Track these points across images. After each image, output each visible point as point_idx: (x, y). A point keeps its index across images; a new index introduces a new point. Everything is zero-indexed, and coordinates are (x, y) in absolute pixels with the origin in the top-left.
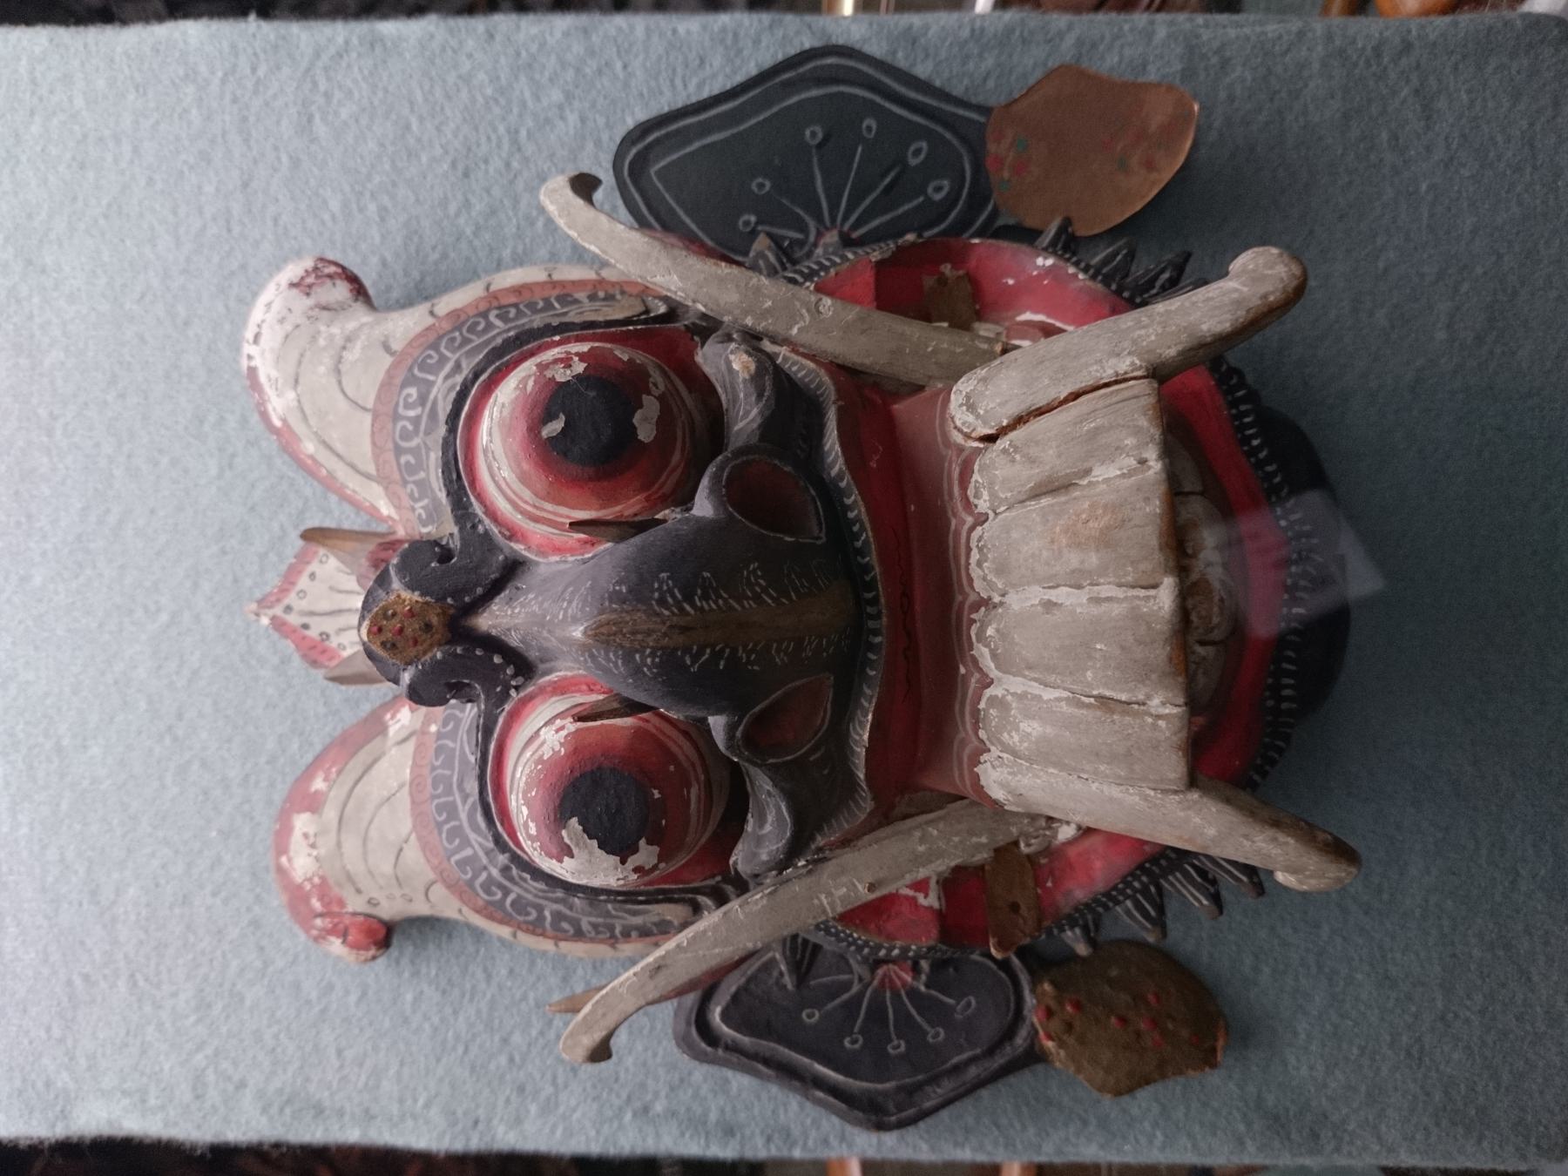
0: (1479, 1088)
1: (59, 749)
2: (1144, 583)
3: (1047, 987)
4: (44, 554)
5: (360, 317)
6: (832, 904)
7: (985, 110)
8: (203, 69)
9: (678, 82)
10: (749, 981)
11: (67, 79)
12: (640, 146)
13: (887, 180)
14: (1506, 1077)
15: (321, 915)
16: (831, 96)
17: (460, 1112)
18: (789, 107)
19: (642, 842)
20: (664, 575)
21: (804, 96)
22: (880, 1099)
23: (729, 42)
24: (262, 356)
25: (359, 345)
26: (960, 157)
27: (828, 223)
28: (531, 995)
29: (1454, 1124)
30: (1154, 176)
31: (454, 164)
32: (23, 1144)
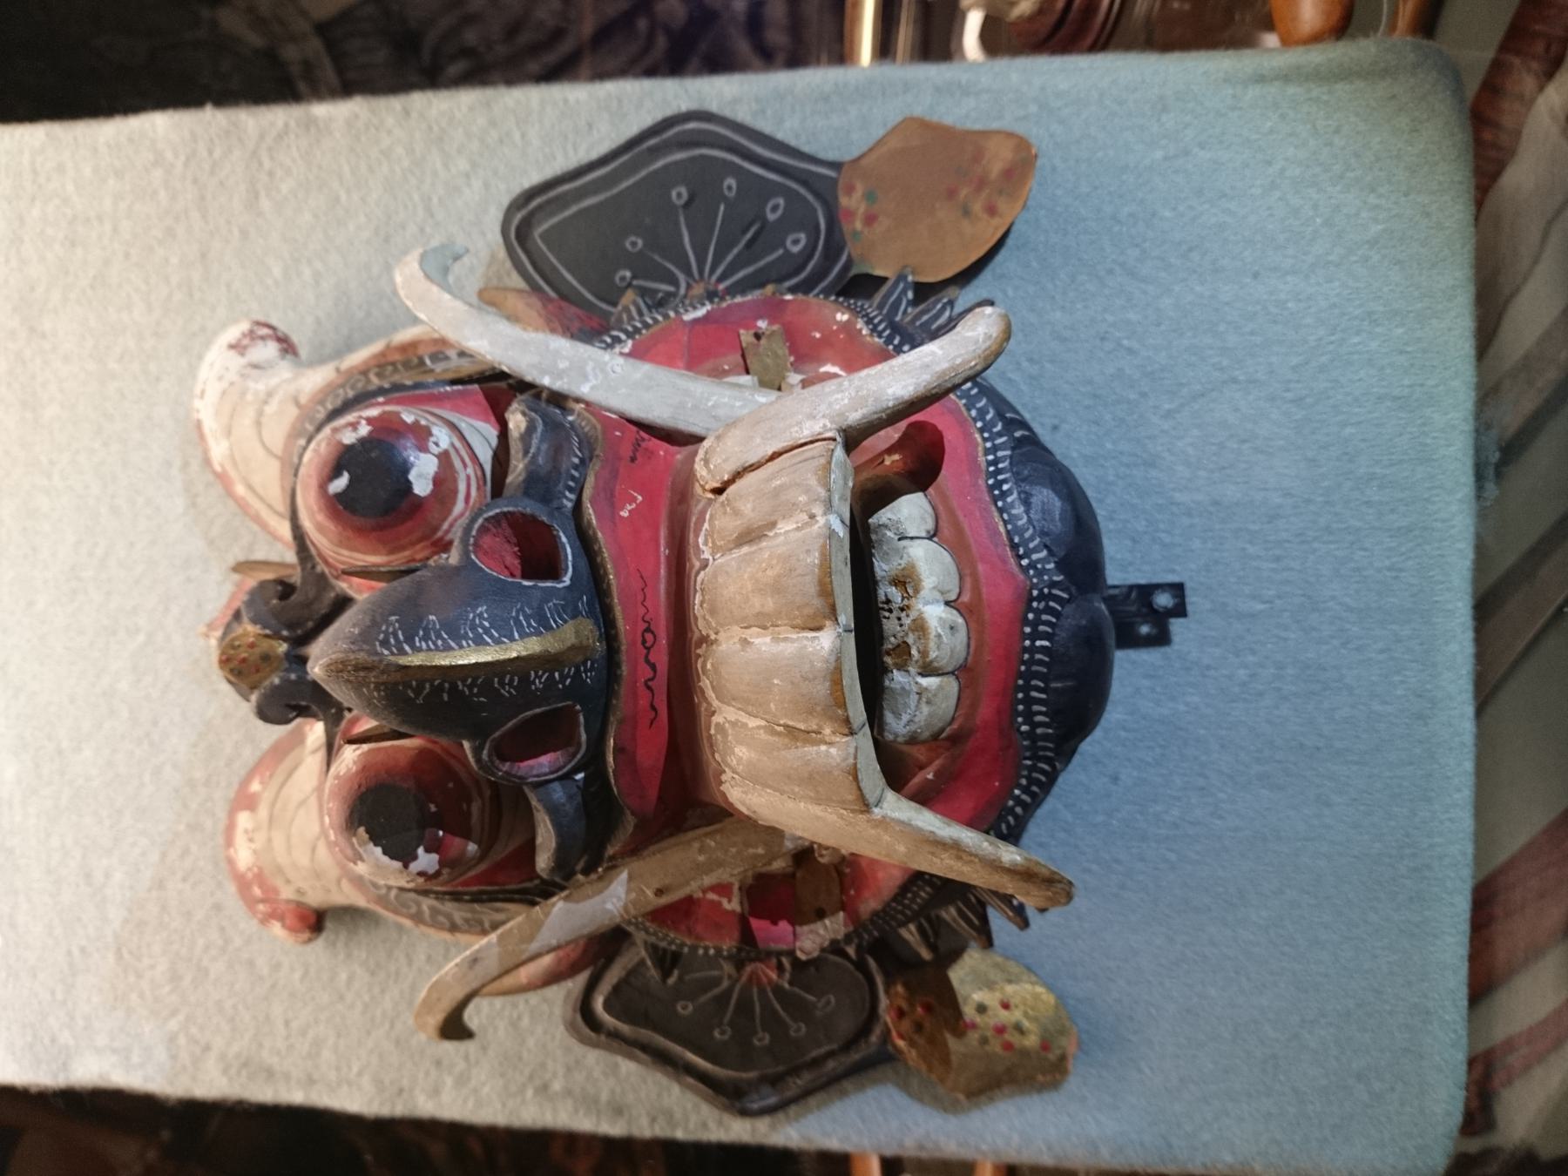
1: (60, 752)
3: (900, 989)
7: (836, 166)
8: (169, 155)
9: (570, 147)
11: (61, 169)
13: (749, 235)
15: (262, 901)
16: (692, 159)
18: (656, 172)
19: (421, 850)
20: (393, 618)
26: (815, 210)
27: (696, 275)
32: (33, 1090)
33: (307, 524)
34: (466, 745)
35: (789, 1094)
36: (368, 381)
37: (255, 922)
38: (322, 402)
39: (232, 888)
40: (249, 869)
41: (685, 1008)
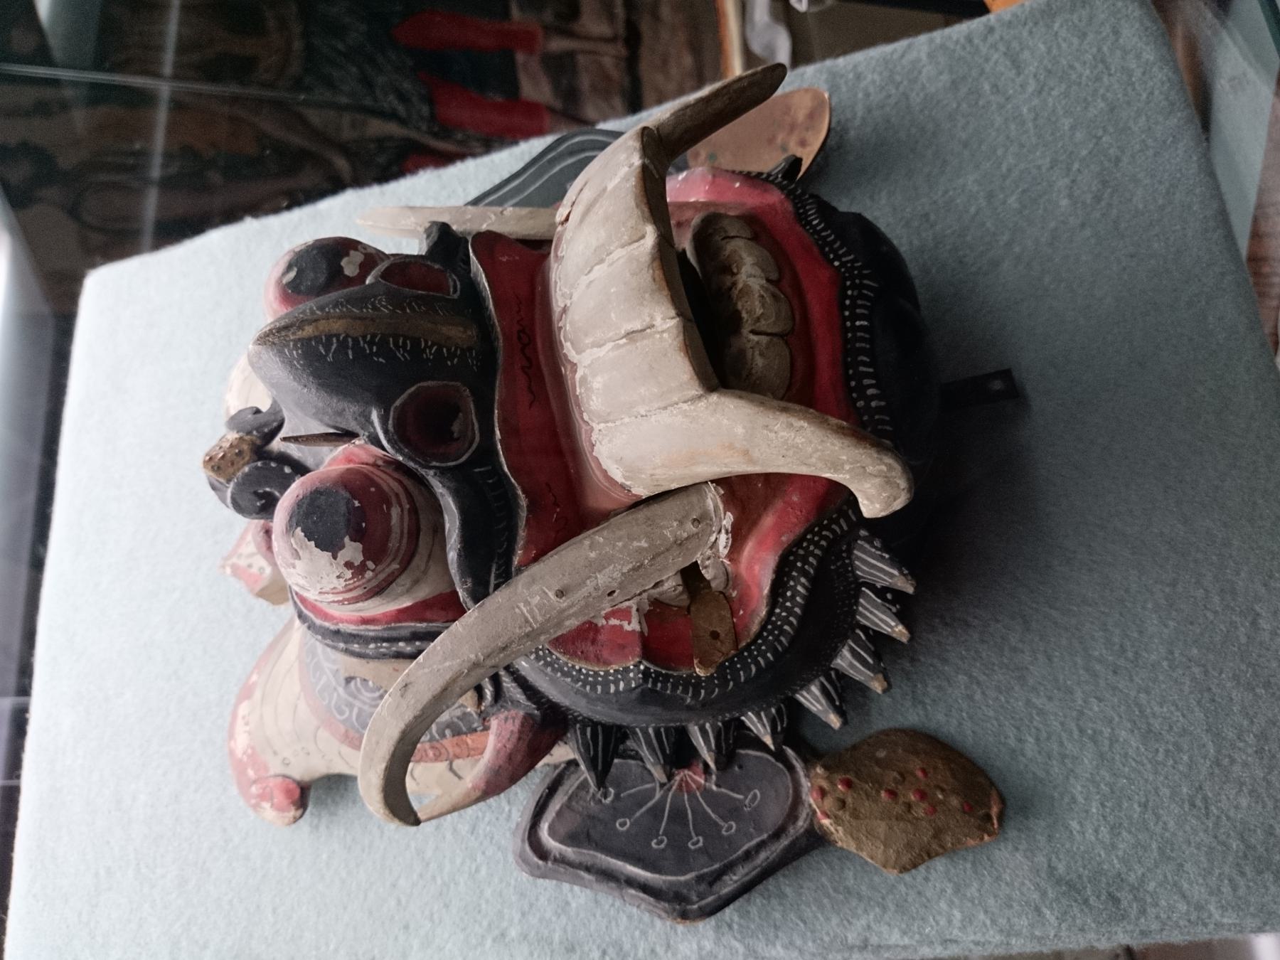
2: (635, 238)
3: (819, 770)
10: (570, 799)
15: (255, 782)
28: (413, 844)
29: (1260, 873)
30: (808, 149)
35: (726, 890)
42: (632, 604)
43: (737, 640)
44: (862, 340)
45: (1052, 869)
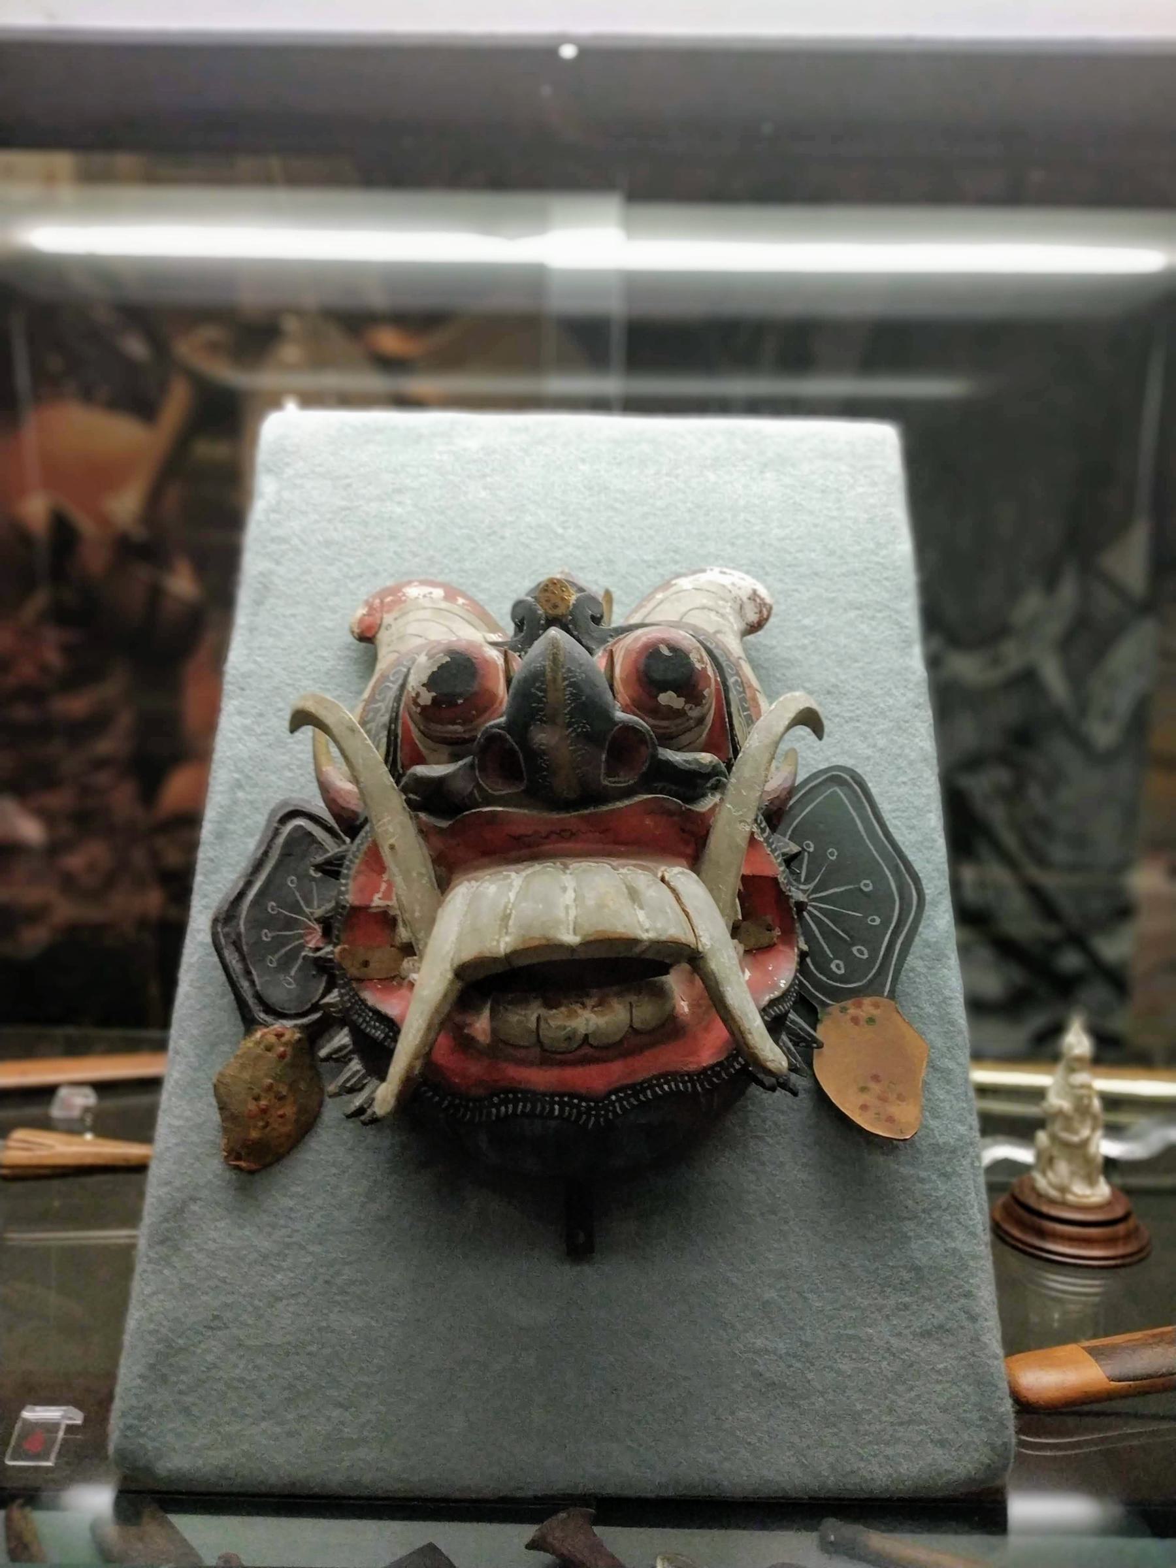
0: (183, 1377)
1: (484, 476)
3: (298, 1036)
4: (598, 471)
5: (738, 626)
6: (384, 824)
9: (898, 814)
11: (874, 484)
12: (851, 781)
14: (188, 1399)
15: (382, 602)
17: (249, 680)
21: (891, 878)
22: (234, 923)
23: (926, 844)
24: (713, 576)
25: (720, 620)
31: (836, 686)
33: (640, 631)
34: (503, 719)
35: (226, 953)
36: (732, 675)
37: (365, 597)
38: (717, 647)
39: (389, 583)
40: (404, 595)
41: (292, 882)
42: (393, 903)
43: (360, 980)
44: (543, 1108)
45: (194, 1200)
